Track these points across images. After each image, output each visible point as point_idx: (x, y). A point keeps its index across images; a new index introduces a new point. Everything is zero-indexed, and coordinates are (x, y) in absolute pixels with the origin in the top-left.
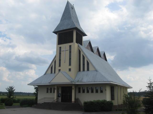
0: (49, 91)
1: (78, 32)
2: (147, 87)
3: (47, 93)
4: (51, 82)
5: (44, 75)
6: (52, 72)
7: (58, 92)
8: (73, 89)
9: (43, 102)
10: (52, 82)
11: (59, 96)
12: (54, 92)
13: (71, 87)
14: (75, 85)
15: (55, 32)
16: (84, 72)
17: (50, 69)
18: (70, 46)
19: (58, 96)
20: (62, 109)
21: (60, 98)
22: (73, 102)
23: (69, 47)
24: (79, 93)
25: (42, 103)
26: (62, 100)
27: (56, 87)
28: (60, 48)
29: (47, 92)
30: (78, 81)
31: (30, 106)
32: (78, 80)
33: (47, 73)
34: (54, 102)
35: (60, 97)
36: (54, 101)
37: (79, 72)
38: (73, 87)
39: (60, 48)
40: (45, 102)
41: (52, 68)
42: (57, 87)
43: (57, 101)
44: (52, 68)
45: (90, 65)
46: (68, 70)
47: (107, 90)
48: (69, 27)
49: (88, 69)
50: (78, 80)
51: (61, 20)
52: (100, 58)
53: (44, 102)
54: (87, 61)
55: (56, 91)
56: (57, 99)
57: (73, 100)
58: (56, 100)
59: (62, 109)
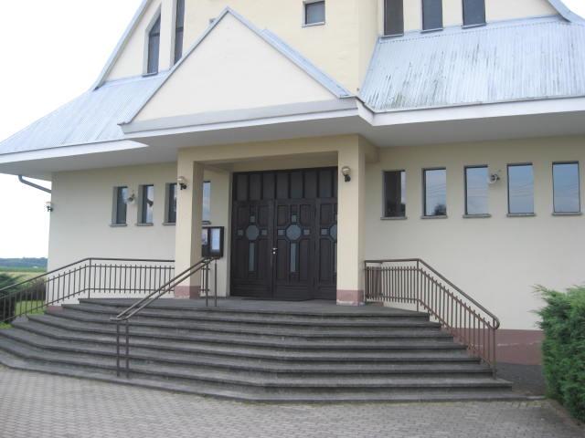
0: (132, 213)
3: (119, 230)
4: (141, 118)
5: (97, 88)
6: (152, 67)
8: (348, 179)
9: (74, 301)
10: (149, 115)
11: (216, 246)
12: (171, 218)
16: (433, 39)
17: (141, 39)
19: (207, 253)
20: (113, 363)
21: (223, 266)
22: (348, 294)
24: (394, 224)
25: (67, 302)
26: (239, 286)
27: (185, 172)
29: (120, 218)
30: (398, 104)
32: (394, 94)
33: (117, 74)
34: (166, 296)
35: (219, 255)
36: (170, 286)
37: (394, 43)
38: (350, 162)
40: (95, 295)
41: (154, 34)
43: (194, 291)
44: (154, 34)
50: (400, 97)
53: (84, 296)
55: (184, 201)
56: (194, 269)
57: (348, 278)
58: (187, 283)
59: (113, 363)
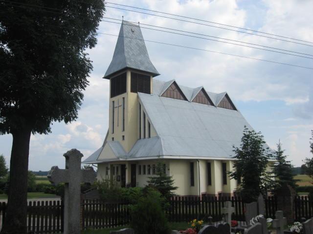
1: (133, 72)
2: (284, 150)
7: (117, 173)
10: (100, 158)
13: (125, 165)
14: (129, 162)
15: (106, 77)
18: (124, 98)
23: (122, 99)
28: (113, 102)
31: (44, 186)
33: (108, 140)
38: (127, 166)
39: (113, 102)
42: (112, 166)
45: (151, 126)
46: (122, 138)
47: (170, 169)
48: (120, 68)
49: (149, 136)
51: (114, 56)
52: (183, 102)
54: (148, 121)
